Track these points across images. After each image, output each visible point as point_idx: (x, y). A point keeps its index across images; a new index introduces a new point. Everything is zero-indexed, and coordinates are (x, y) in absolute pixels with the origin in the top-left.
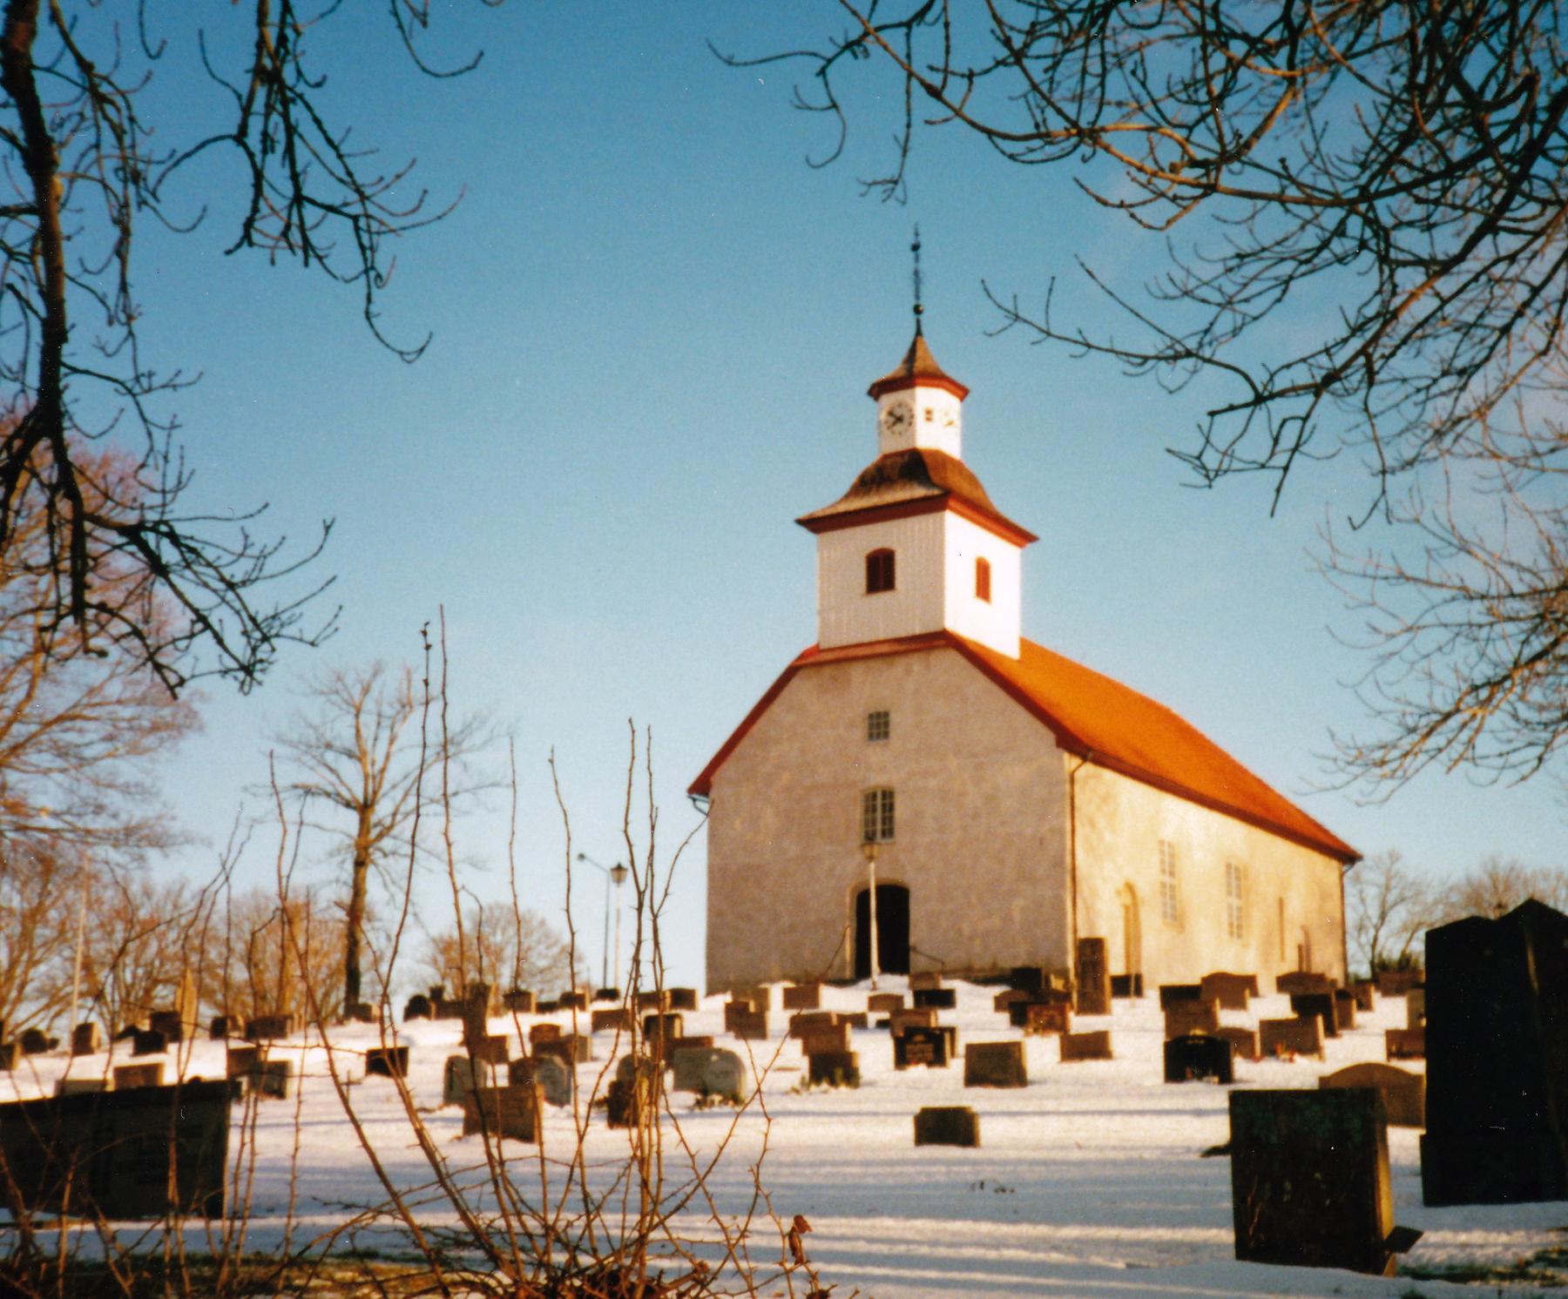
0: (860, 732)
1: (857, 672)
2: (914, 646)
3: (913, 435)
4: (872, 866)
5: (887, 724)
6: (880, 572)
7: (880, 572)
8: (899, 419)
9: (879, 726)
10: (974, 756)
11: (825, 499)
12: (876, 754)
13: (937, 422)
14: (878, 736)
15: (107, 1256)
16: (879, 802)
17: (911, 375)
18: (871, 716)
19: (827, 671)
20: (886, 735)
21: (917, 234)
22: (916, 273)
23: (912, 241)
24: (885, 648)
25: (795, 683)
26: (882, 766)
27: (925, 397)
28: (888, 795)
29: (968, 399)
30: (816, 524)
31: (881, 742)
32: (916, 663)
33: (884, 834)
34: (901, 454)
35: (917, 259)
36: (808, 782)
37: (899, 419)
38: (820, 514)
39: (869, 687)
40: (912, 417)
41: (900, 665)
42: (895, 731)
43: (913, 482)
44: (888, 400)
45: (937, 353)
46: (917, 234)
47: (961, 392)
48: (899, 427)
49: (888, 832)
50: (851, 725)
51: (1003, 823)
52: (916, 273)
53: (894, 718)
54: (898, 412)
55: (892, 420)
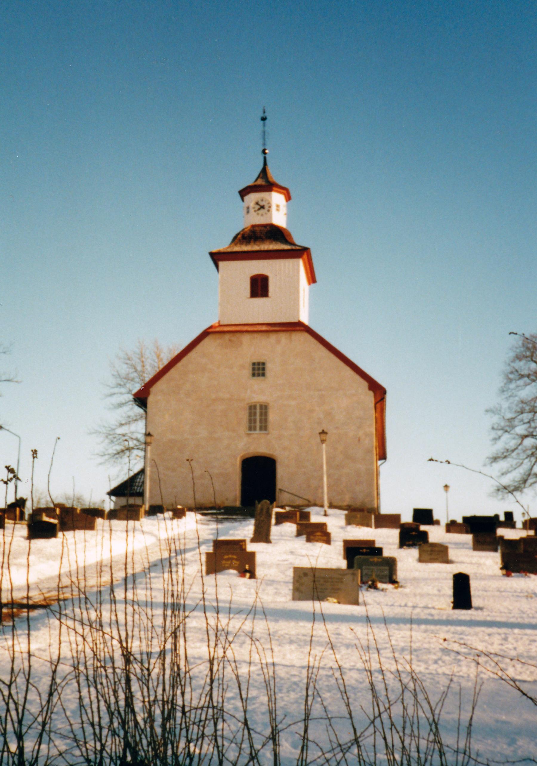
0: (248, 371)
1: (246, 339)
2: (271, 329)
3: (271, 217)
4: (324, 445)
5: (264, 369)
6: (259, 287)
7: (259, 287)
8: (262, 207)
9: (259, 370)
10: (320, 390)
11: (223, 244)
12: (257, 383)
13: (279, 211)
14: (259, 375)
15: (18, 641)
16: (258, 411)
17: (265, 184)
18: (254, 364)
19: (227, 337)
20: (263, 375)
21: (264, 112)
22: (264, 132)
23: (261, 115)
24: (264, 328)
25: (206, 342)
26: (259, 391)
27: (277, 198)
28: (265, 408)
29: (289, 202)
30: (217, 257)
31: (261, 378)
32: (283, 337)
33: (261, 429)
34: (265, 226)
35: (264, 125)
36: (214, 396)
37: (262, 207)
38: (223, 251)
39: (254, 348)
40: (270, 207)
41: (273, 337)
42: (268, 372)
43: (265, 242)
44: (252, 198)
45: (274, 175)
46: (264, 112)
47: (288, 198)
48: (262, 211)
49: (264, 427)
50: (243, 367)
51: (337, 428)
52: (264, 132)
53: (269, 366)
54: (262, 203)
55: (257, 207)
